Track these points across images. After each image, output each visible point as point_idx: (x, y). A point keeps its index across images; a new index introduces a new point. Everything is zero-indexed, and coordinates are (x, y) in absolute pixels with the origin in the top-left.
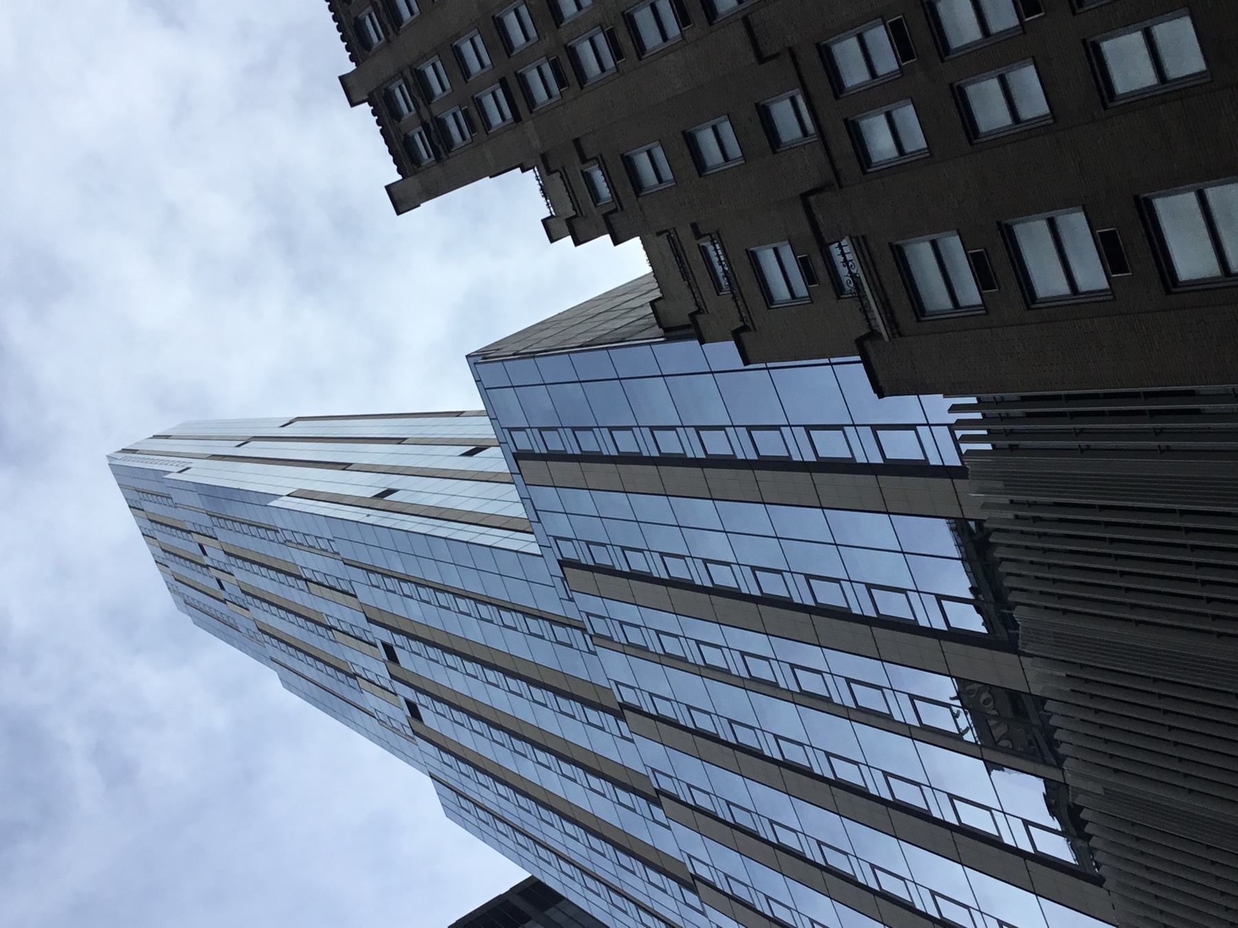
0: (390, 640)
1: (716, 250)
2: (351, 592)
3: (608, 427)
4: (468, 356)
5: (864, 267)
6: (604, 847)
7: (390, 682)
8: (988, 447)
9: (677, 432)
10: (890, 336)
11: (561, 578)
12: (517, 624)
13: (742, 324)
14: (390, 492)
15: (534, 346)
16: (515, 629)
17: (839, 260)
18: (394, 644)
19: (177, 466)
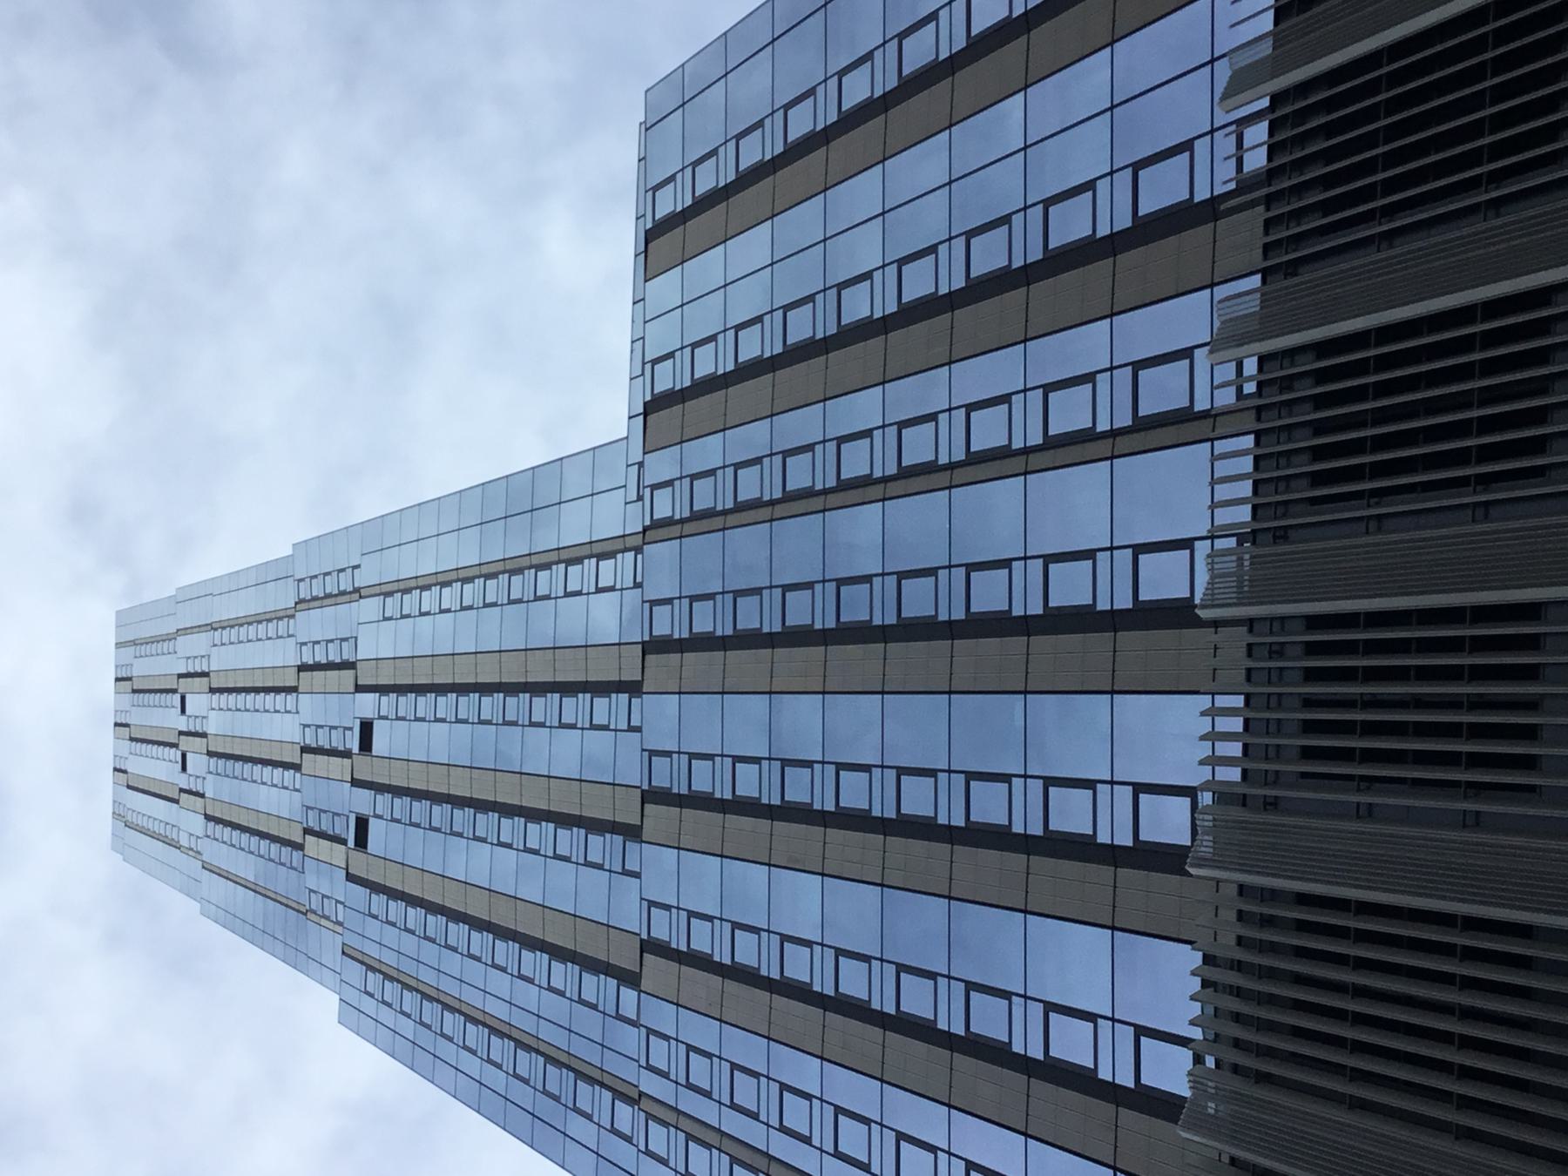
3: (781, 1084)
9: (870, 1129)
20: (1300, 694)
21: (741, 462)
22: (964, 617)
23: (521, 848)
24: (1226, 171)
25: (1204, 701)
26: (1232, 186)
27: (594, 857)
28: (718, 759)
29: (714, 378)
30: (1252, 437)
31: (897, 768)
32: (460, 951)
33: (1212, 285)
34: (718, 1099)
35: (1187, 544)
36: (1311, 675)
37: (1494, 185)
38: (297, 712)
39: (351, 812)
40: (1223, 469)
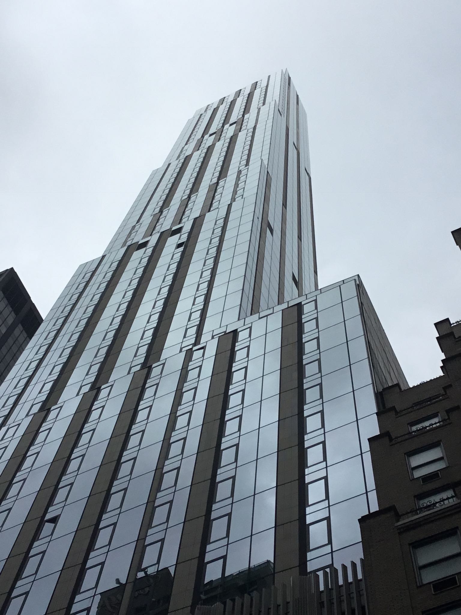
0: (184, 231)
1: (436, 423)
2: (211, 208)
4: (358, 275)
5: (441, 512)
6: (31, 370)
7: (159, 232)
8: (322, 588)
10: (399, 527)
11: (226, 331)
12: (197, 306)
13: (393, 437)
14: (272, 231)
15: (367, 315)
16: (193, 304)
17: (444, 495)
18: (182, 234)
19: (282, 108)
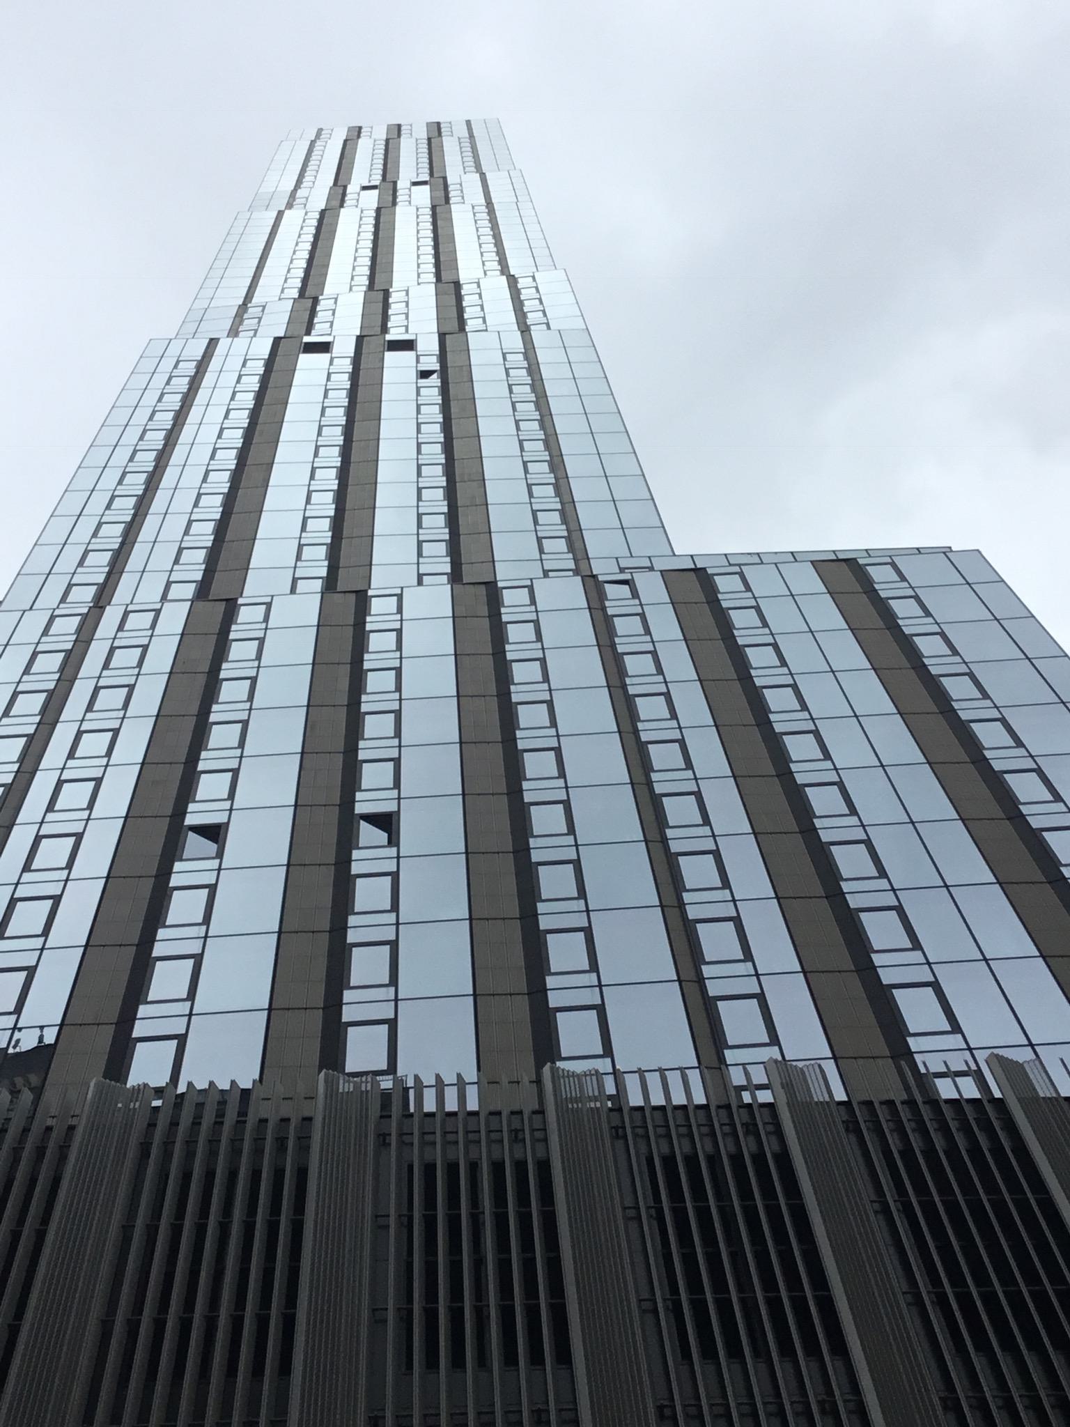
9: (62, 869)
20: (481, 1159)
21: (658, 656)
22: (533, 861)
23: (325, 405)
24: (936, 1065)
25: (471, 1075)
26: (923, 1070)
27: (315, 497)
28: (396, 742)
29: (747, 667)
30: (704, 1102)
31: (401, 667)
32: (204, 485)
33: (835, 1058)
34: (86, 718)
35: (608, 1051)
36: (498, 1168)
37: (935, 1300)
38: (419, 284)
39: (334, 337)
40: (674, 1079)
